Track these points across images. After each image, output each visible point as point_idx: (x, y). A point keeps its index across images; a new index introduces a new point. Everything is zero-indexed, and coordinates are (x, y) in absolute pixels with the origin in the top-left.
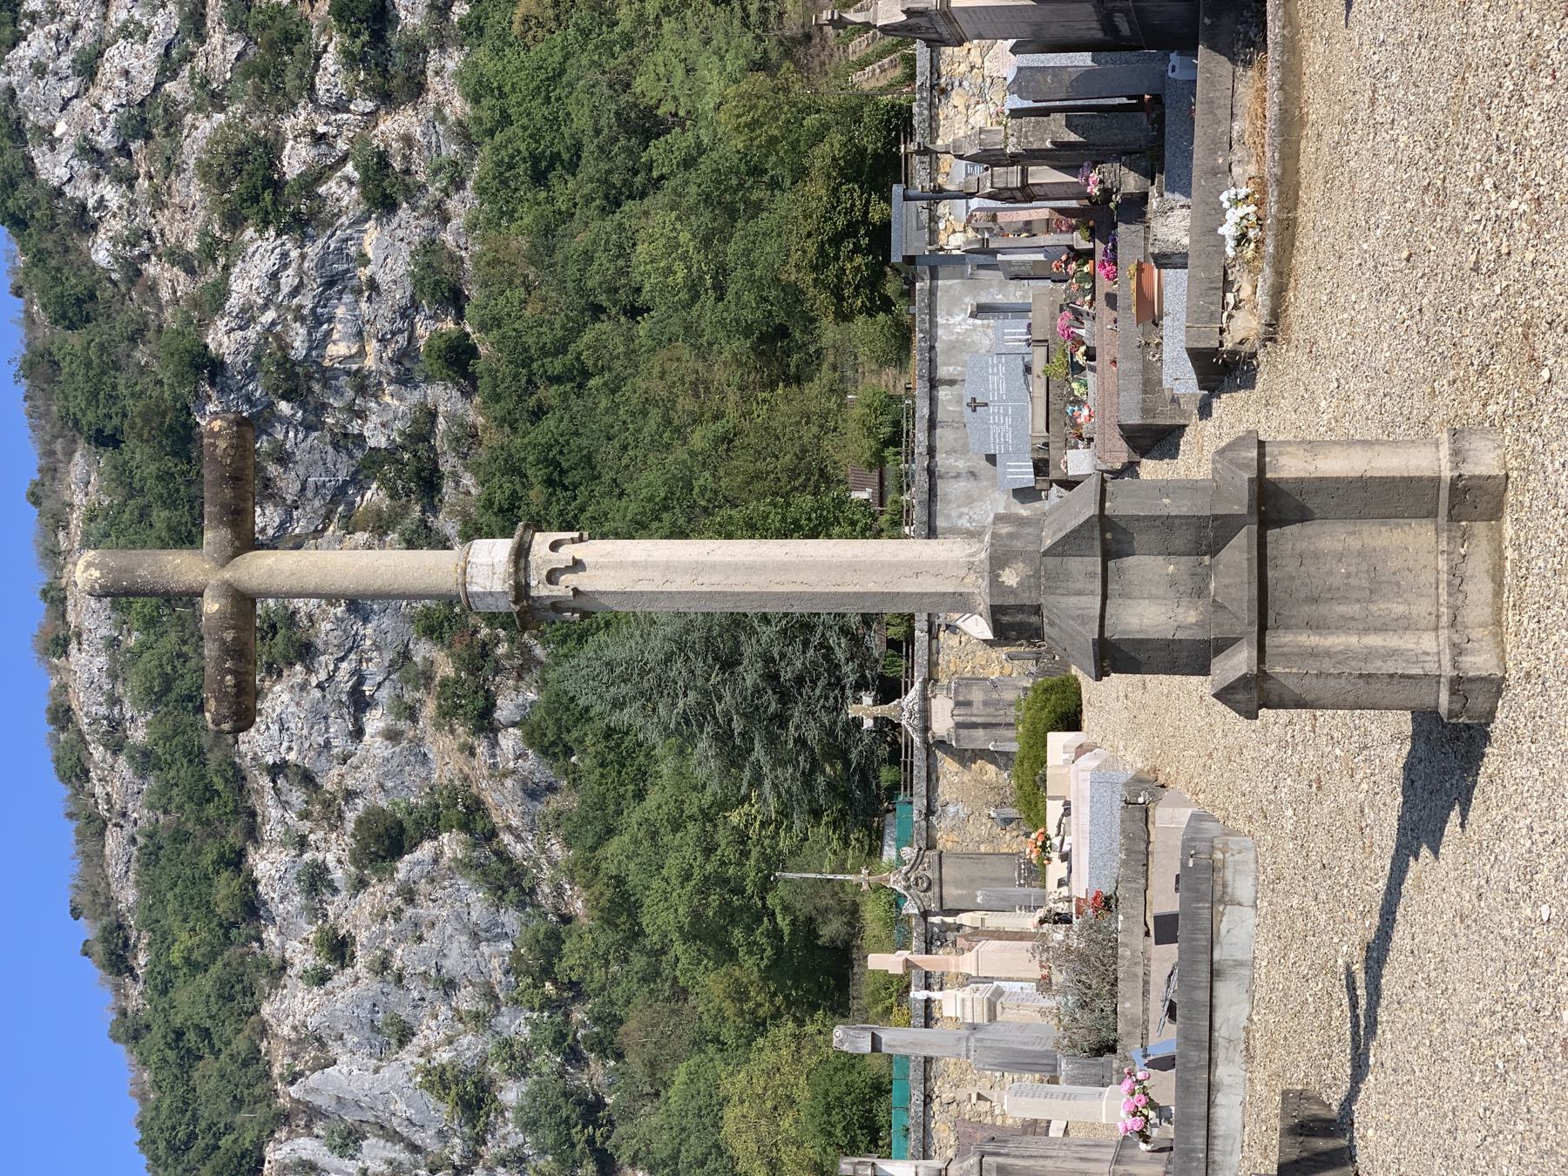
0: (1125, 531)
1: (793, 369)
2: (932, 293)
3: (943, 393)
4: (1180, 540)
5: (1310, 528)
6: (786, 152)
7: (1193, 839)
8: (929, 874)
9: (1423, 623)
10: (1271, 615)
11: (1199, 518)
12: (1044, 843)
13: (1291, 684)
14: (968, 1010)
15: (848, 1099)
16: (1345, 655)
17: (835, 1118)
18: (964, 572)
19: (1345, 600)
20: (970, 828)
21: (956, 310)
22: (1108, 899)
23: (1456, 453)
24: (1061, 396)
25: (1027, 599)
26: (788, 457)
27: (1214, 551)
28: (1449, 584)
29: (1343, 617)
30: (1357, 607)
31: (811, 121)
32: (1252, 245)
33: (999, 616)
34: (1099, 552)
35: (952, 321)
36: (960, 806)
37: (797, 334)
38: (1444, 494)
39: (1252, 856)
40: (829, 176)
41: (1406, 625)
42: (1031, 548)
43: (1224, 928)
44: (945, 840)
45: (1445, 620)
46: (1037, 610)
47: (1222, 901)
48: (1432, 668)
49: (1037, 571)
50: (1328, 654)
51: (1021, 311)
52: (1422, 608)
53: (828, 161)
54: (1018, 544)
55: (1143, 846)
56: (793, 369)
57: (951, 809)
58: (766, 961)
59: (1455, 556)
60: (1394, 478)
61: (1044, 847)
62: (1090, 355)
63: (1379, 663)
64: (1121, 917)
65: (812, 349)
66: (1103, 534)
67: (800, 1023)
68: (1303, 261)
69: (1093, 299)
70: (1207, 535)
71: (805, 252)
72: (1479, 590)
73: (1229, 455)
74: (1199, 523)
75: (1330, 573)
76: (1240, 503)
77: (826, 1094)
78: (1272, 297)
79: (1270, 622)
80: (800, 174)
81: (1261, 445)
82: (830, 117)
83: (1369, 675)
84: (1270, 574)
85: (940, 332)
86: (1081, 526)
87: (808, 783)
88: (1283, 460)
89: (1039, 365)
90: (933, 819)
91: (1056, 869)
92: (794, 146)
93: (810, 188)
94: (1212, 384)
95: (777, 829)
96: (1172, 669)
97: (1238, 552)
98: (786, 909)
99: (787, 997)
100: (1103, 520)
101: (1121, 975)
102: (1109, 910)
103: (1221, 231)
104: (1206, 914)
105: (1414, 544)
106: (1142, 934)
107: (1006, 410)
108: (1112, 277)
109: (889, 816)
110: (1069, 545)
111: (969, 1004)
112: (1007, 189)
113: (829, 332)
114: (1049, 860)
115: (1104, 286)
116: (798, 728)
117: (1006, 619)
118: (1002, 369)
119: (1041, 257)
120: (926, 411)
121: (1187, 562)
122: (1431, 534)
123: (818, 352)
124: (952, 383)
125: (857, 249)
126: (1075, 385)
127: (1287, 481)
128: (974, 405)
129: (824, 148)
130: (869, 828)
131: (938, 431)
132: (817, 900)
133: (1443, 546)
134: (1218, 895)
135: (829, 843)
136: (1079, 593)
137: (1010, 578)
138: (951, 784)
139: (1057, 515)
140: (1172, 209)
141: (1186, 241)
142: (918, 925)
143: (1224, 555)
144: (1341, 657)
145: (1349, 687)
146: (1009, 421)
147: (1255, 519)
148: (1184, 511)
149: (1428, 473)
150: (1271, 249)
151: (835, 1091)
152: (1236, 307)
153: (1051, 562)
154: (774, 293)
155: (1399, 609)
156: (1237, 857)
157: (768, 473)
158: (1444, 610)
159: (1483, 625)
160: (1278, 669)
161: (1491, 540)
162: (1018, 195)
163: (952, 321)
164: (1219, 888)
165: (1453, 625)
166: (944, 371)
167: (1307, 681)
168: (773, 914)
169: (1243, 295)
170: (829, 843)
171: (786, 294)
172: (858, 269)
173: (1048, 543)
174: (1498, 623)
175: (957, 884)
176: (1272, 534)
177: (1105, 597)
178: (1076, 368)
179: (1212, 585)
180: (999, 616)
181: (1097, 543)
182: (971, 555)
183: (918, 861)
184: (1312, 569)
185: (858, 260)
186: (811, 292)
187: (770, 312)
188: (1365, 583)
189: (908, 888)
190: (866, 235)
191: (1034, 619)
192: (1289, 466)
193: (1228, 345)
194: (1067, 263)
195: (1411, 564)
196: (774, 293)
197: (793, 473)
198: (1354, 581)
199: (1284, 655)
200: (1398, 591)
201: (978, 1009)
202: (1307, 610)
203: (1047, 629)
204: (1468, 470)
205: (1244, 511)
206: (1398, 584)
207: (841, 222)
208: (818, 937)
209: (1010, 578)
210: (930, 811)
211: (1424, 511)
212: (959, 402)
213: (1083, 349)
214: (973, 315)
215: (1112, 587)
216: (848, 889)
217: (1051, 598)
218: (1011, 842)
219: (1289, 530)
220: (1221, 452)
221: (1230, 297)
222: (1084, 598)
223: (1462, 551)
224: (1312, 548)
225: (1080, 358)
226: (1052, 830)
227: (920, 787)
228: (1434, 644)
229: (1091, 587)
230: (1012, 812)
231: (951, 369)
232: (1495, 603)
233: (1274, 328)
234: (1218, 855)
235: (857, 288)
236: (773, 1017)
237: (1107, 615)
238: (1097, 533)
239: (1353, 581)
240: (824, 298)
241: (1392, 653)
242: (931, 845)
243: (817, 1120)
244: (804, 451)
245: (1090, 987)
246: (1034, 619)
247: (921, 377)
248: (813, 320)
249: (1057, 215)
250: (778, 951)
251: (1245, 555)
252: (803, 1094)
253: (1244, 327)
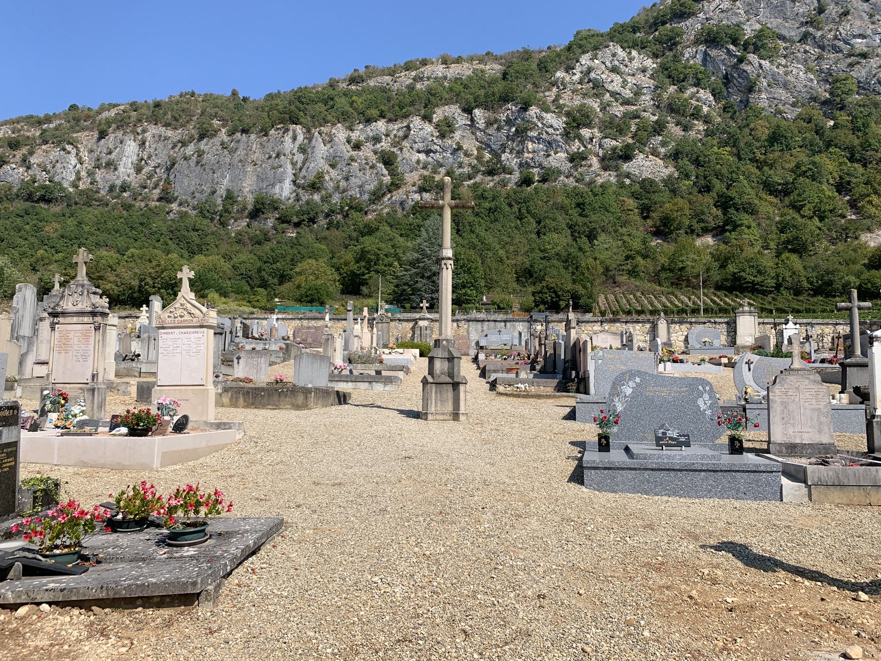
3: (503, 324)
16: (431, 396)
31: (589, 285)
41: (436, 406)
44: (392, 324)
70: (451, 375)
72: (442, 417)
87: (406, 284)
97: (448, 380)
110: (450, 352)
113: (531, 289)
125: (552, 298)
128: (500, 331)
137: (444, 342)
166: (508, 324)
183: (388, 317)
192: (462, 388)
207: (560, 293)
209: (444, 342)
242: (391, 320)
250: (359, 275)
252: (319, 282)
253: (500, 388)
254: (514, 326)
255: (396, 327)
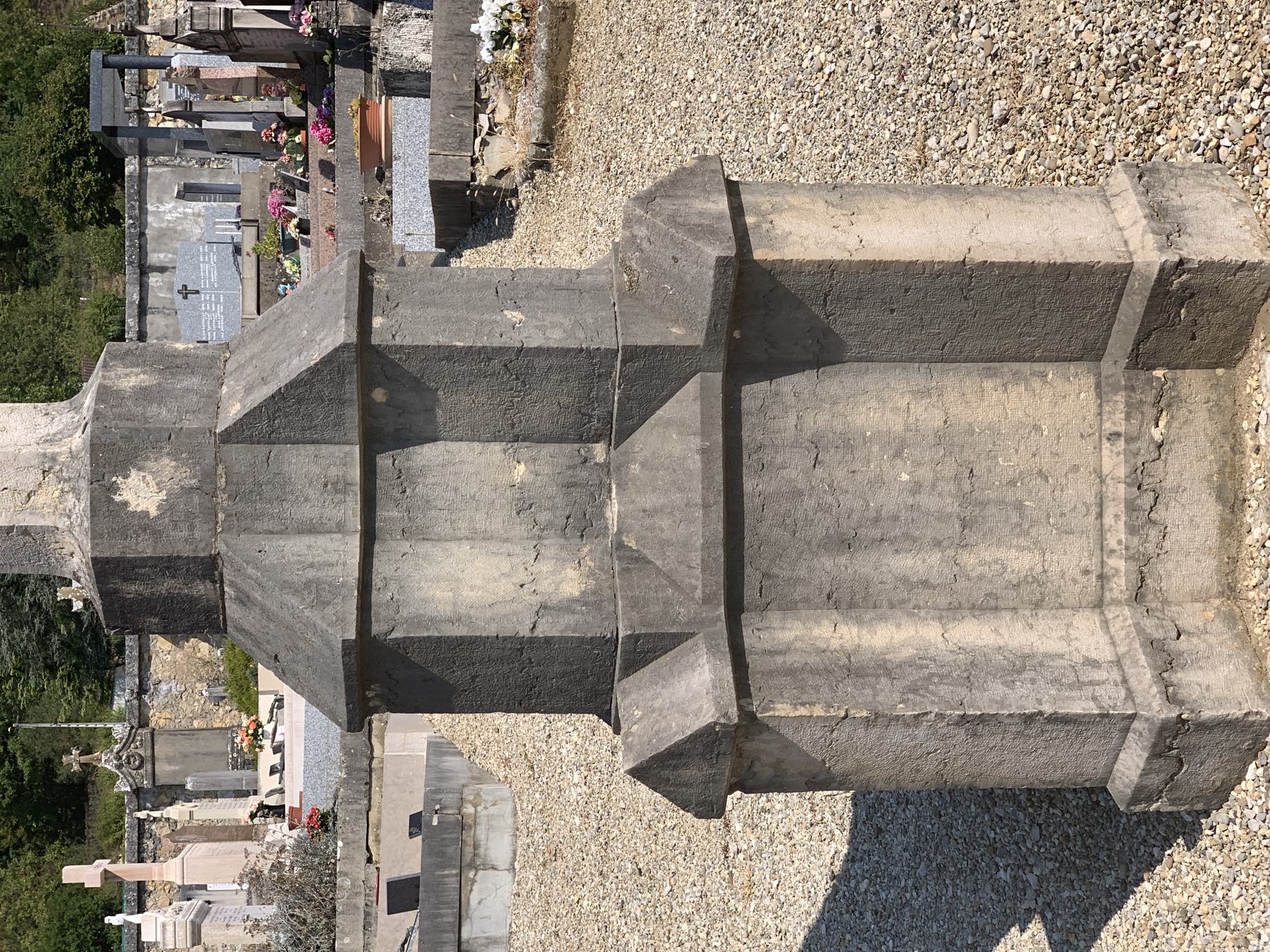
0: (418, 385)
1: (31, 274)
2: (142, 178)
3: (154, 280)
4: (542, 407)
5: (834, 382)
6: (21, 77)
7: (438, 791)
8: (141, 752)
9: (1071, 593)
10: (751, 576)
11: (590, 354)
12: (256, 730)
13: (806, 740)
14: (170, 935)
15: (82, 921)
16: (919, 673)
17: (69, 938)
18: (33, 477)
19: (909, 542)
20: (183, 705)
21: (166, 198)
22: (324, 816)
23: (1158, 213)
24: (273, 277)
25: (181, 543)
26: (26, 352)
27: (620, 429)
28: (1131, 507)
29: (904, 580)
30: (935, 558)
31: (43, 50)
32: (516, 46)
33: (116, 583)
34: (355, 435)
35: (162, 209)
36: (173, 684)
37: (35, 244)
38: (1133, 307)
39: (508, 808)
40: (61, 100)
41: (1036, 597)
42: (191, 423)
43: (474, 898)
44: (158, 718)
45: (1120, 586)
46: (209, 568)
47: (473, 866)
48: (1112, 698)
49: (209, 476)
50: (883, 668)
51: (231, 193)
52: (1069, 559)
53: (60, 86)
54: (162, 414)
55: (365, 763)
56: (31, 274)
57: (164, 687)
58: (7, 800)
59: (1142, 444)
60: (1033, 265)
61: (255, 735)
62: (304, 227)
63: (997, 689)
64: (340, 844)
65: (49, 257)
66: (365, 392)
67: (40, 851)
68: (590, 57)
69: (306, 170)
70: (597, 397)
71: (38, 167)
72: (1191, 519)
73: (668, 206)
74: (586, 365)
75: (879, 482)
76: (687, 320)
77: (61, 917)
78: (545, 108)
79: (750, 594)
80: (35, 96)
81: (733, 189)
82: (61, 48)
83: (983, 719)
84: (749, 485)
85: (150, 219)
86: (314, 371)
87: (43, 641)
88: (784, 223)
89: (249, 244)
90: (146, 698)
91: (267, 758)
92: (29, 72)
93: (44, 110)
94: (452, 240)
95: (15, 684)
96: (524, 699)
97: (676, 436)
98: (25, 752)
99: (28, 829)
100: (366, 361)
101: (339, 908)
102: (327, 830)
103: (474, 28)
104: (452, 883)
105: (1048, 416)
106: (364, 861)
107: (217, 297)
108: (329, 140)
109: (120, 668)
110: (286, 415)
111: (170, 928)
112: (209, 32)
113: (65, 242)
114: (261, 747)
115: (319, 152)
116: (33, 593)
117: (132, 589)
118: (214, 258)
119: (248, 126)
120: (136, 297)
121: (553, 456)
122: (1088, 396)
123: (55, 260)
124: (162, 270)
125: (87, 166)
126: (287, 263)
127: (798, 268)
128: (185, 292)
129: (55, 75)
130: (101, 680)
131: (149, 317)
132: (55, 743)
133: (1116, 420)
134: (468, 858)
135: (64, 694)
136: (311, 529)
137: (141, 493)
138: (164, 662)
139: (256, 347)
140: (405, 17)
141: (426, 58)
142: (130, 801)
143: (645, 440)
144: (915, 675)
145: (932, 744)
146: (220, 308)
147: (720, 358)
148: (556, 338)
149: (1105, 257)
150: (543, 45)
151: (70, 914)
152: (491, 132)
153: (239, 454)
154: (13, 206)
155: (1021, 561)
156: (492, 810)
157: (7, 365)
158: (1117, 562)
159: (1201, 597)
160: (783, 709)
161: (1216, 408)
162: (222, 41)
163: (162, 209)
164: (469, 850)
165: (1138, 596)
166: (154, 258)
167: (841, 734)
168: (14, 757)
169: (499, 118)
170: (64, 694)
171: (25, 207)
172: (88, 184)
173: (234, 411)
174: (1231, 591)
175: (169, 760)
176: (754, 394)
177: (369, 538)
178: (290, 246)
179: (613, 511)
180: (116, 583)
181: (352, 415)
182: (50, 440)
183: (130, 739)
184: (840, 474)
185: (89, 176)
186: (44, 204)
187: (10, 223)
188: (952, 506)
189: (119, 767)
190: (96, 154)
191: (202, 589)
192: (803, 234)
193: (482, 179)
194: (277, 130)
195: (1045, 461)
196: (13, 206)
197: (32, 366)
198: (926, 500)
199: (790, 672)
200: (1021, 522)
201: (180, 933)
202: (830, 565)
203: (233, 610)
204: (1197, 249)
205: (697, 339)
206: (1019, 506)
207: (72, 141)
208: (56, 776)
209: (141, 493)
210: (142, 690)
211: (1076, 346)
212: (170, 289)
213: (295, 221)
214: (180, 196)
215: (387, 513)
216: (83, 734)
217: (244, 543)
218: (226, 715)
219: (789, 384)
220: (646, 199)
221: (483, 119)
222: (321, 541)
223: (1157, 434)
224: (839, 425)
225: (292, 231)
226: (264, 716)
227: (132, 667)
228: (1103, 639)
229: (335, 514)
230: (220, 690)
231: (162, 256)
232: (1224, 547)
233: (543, 159)
234: (469, 809)
235: (87, 201)
236: (16, 847)
237: (377, 581)
238: (351, 390)
239: (926, 500)
240: (56, 209)
241: (1020, 665)
242: (144, 723)
243: (53, 942)
244: (41, 346)
245: (304, 922)
246: (202, 589)
247: (131, 263)
248: (49, 231)
249: (265, 75)
250: (19, 790)
251: (696, 442)
252: (42, 917)
253: (503, 154)
254: (162, 234)
255: (173, 703)
